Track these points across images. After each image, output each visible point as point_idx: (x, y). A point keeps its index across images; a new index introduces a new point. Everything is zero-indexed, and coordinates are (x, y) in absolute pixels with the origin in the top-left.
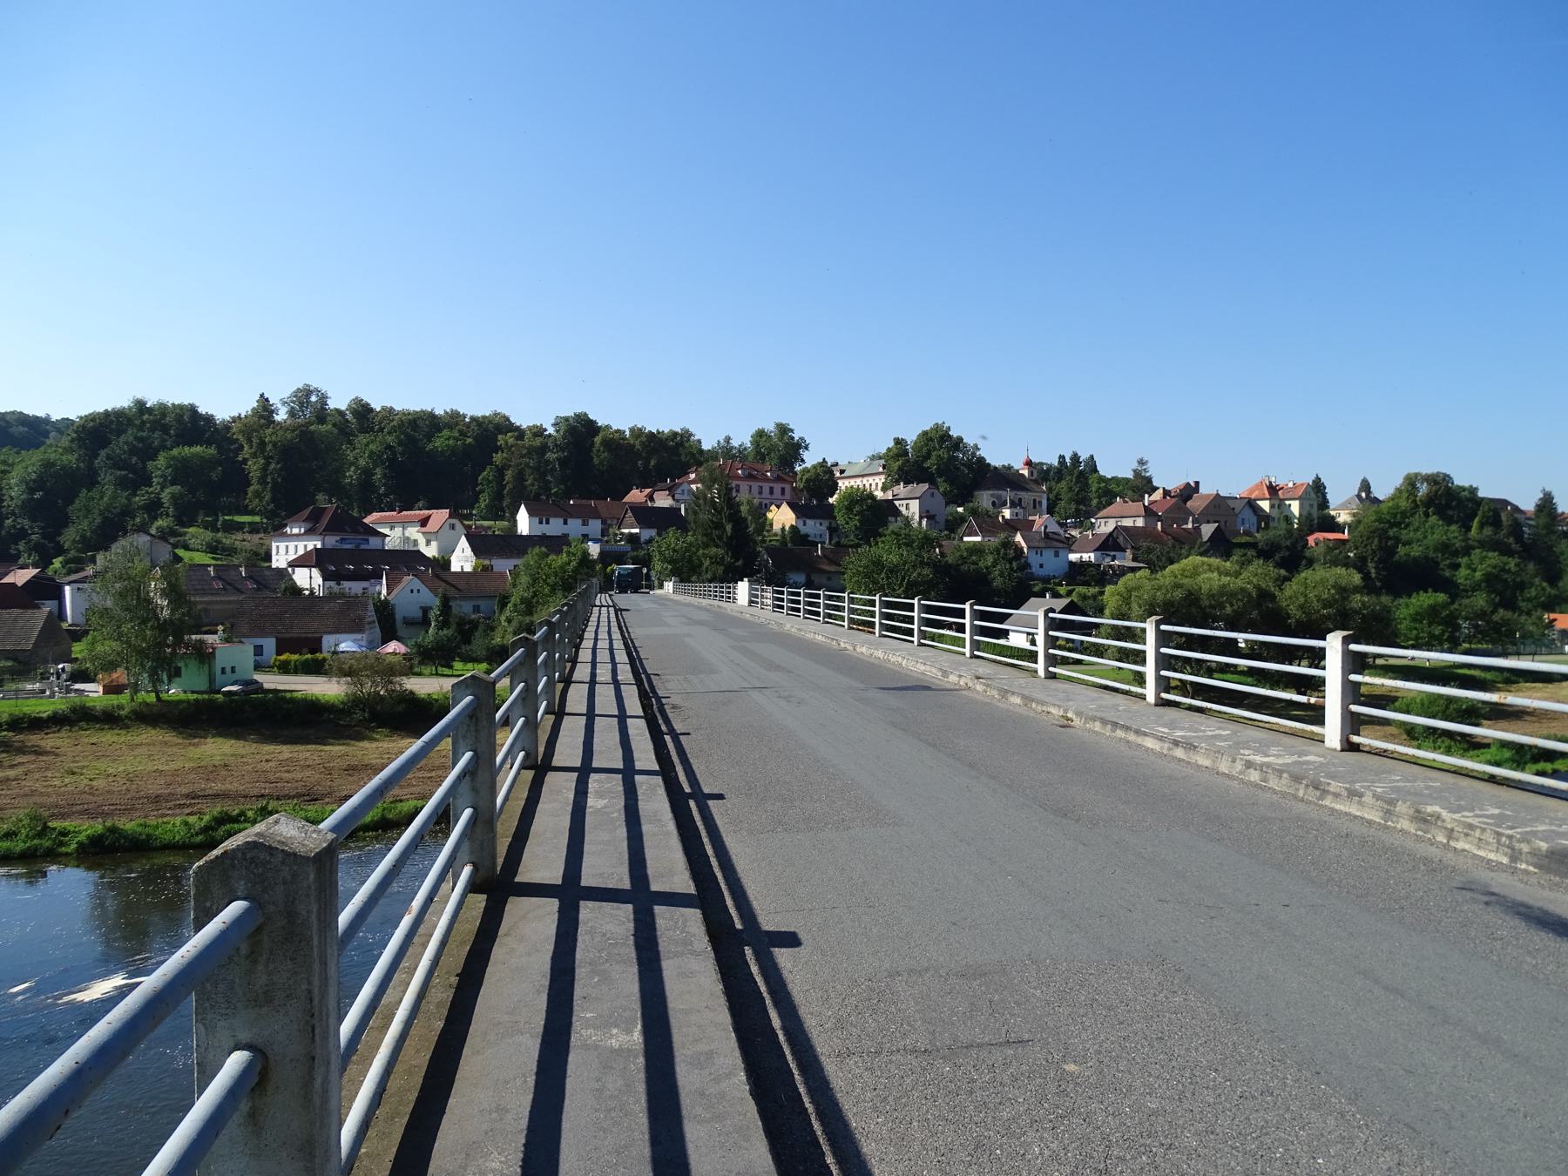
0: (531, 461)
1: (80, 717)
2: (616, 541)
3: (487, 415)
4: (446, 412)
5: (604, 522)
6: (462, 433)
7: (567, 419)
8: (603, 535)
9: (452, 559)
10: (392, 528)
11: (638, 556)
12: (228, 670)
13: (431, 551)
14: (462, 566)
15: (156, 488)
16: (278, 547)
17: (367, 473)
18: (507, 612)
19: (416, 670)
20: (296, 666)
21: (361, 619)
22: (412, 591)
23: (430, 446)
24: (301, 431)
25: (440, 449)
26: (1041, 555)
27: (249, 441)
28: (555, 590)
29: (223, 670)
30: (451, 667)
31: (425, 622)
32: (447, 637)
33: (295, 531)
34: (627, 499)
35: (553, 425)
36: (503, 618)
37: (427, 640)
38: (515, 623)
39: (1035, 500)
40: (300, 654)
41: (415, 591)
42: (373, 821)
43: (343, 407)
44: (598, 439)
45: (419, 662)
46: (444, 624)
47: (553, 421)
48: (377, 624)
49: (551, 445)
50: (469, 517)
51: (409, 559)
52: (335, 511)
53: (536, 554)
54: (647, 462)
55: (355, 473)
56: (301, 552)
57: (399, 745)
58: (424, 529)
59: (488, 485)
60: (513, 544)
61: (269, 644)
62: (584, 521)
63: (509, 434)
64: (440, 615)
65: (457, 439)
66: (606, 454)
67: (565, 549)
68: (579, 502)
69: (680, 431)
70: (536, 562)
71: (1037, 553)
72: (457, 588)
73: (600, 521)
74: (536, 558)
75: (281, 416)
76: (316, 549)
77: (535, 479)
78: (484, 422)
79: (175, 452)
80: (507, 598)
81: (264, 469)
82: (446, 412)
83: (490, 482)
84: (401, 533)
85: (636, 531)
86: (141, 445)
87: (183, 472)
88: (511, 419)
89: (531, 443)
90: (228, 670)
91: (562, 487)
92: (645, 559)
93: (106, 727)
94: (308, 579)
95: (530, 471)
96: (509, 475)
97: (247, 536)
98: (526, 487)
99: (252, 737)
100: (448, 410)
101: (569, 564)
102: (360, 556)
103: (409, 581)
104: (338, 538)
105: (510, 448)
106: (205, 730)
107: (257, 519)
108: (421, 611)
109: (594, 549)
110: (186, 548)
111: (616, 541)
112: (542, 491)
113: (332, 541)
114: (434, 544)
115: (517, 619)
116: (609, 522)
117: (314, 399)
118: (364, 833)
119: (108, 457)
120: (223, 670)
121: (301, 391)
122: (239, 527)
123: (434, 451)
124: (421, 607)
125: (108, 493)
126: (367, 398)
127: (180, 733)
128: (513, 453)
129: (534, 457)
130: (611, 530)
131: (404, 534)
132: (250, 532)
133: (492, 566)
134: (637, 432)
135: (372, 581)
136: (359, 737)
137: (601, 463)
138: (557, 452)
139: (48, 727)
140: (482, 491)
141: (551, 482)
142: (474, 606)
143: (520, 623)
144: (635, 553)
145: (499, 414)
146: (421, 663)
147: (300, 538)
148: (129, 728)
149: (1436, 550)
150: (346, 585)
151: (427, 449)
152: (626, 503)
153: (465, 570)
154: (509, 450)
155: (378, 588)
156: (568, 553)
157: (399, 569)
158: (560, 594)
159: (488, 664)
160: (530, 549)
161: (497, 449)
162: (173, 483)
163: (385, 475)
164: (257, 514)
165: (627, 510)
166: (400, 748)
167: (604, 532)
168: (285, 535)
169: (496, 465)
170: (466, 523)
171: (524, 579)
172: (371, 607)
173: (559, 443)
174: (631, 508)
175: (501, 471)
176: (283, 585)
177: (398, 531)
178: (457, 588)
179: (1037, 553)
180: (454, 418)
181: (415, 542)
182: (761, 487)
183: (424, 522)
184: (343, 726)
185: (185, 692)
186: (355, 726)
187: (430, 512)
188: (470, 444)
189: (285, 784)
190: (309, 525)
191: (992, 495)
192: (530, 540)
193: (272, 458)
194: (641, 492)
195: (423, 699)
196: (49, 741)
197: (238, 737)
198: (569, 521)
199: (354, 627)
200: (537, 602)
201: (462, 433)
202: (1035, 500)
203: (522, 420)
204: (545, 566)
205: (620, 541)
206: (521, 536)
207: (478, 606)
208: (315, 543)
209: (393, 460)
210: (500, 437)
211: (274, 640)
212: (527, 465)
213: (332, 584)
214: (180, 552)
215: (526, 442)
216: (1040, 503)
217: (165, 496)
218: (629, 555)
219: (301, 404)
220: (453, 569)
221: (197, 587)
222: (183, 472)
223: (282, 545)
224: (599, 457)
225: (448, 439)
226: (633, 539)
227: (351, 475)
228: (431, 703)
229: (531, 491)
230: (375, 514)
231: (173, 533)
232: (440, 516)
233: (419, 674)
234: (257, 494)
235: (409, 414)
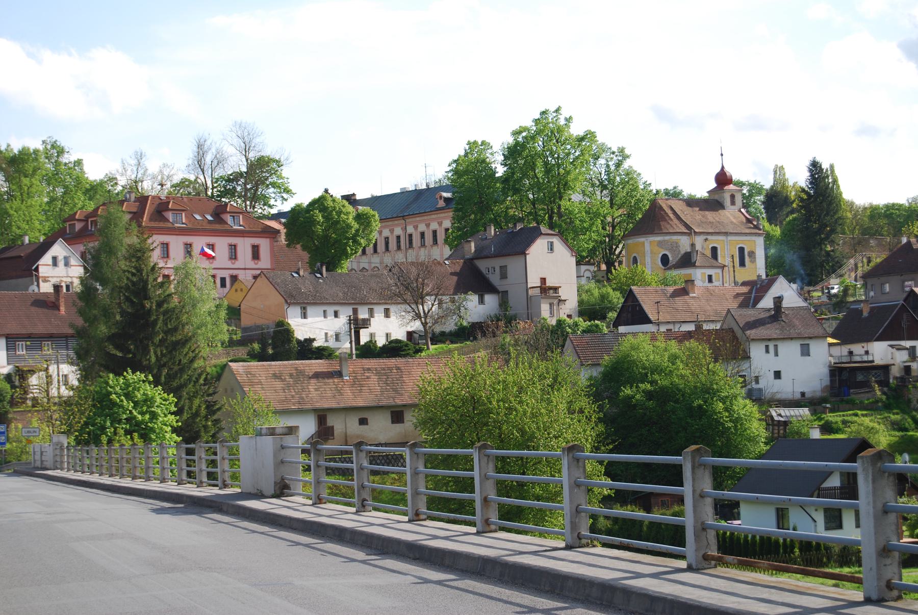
26: (776, 354)
39: (741, 250)
69: (41, 147)
71: (767, 351)
126: (597, 134)
149: (831, 390)
179: (767, 351)
182: (552, 244)
191: (660, 244)
202: (741, 250)
216: (752, 254)
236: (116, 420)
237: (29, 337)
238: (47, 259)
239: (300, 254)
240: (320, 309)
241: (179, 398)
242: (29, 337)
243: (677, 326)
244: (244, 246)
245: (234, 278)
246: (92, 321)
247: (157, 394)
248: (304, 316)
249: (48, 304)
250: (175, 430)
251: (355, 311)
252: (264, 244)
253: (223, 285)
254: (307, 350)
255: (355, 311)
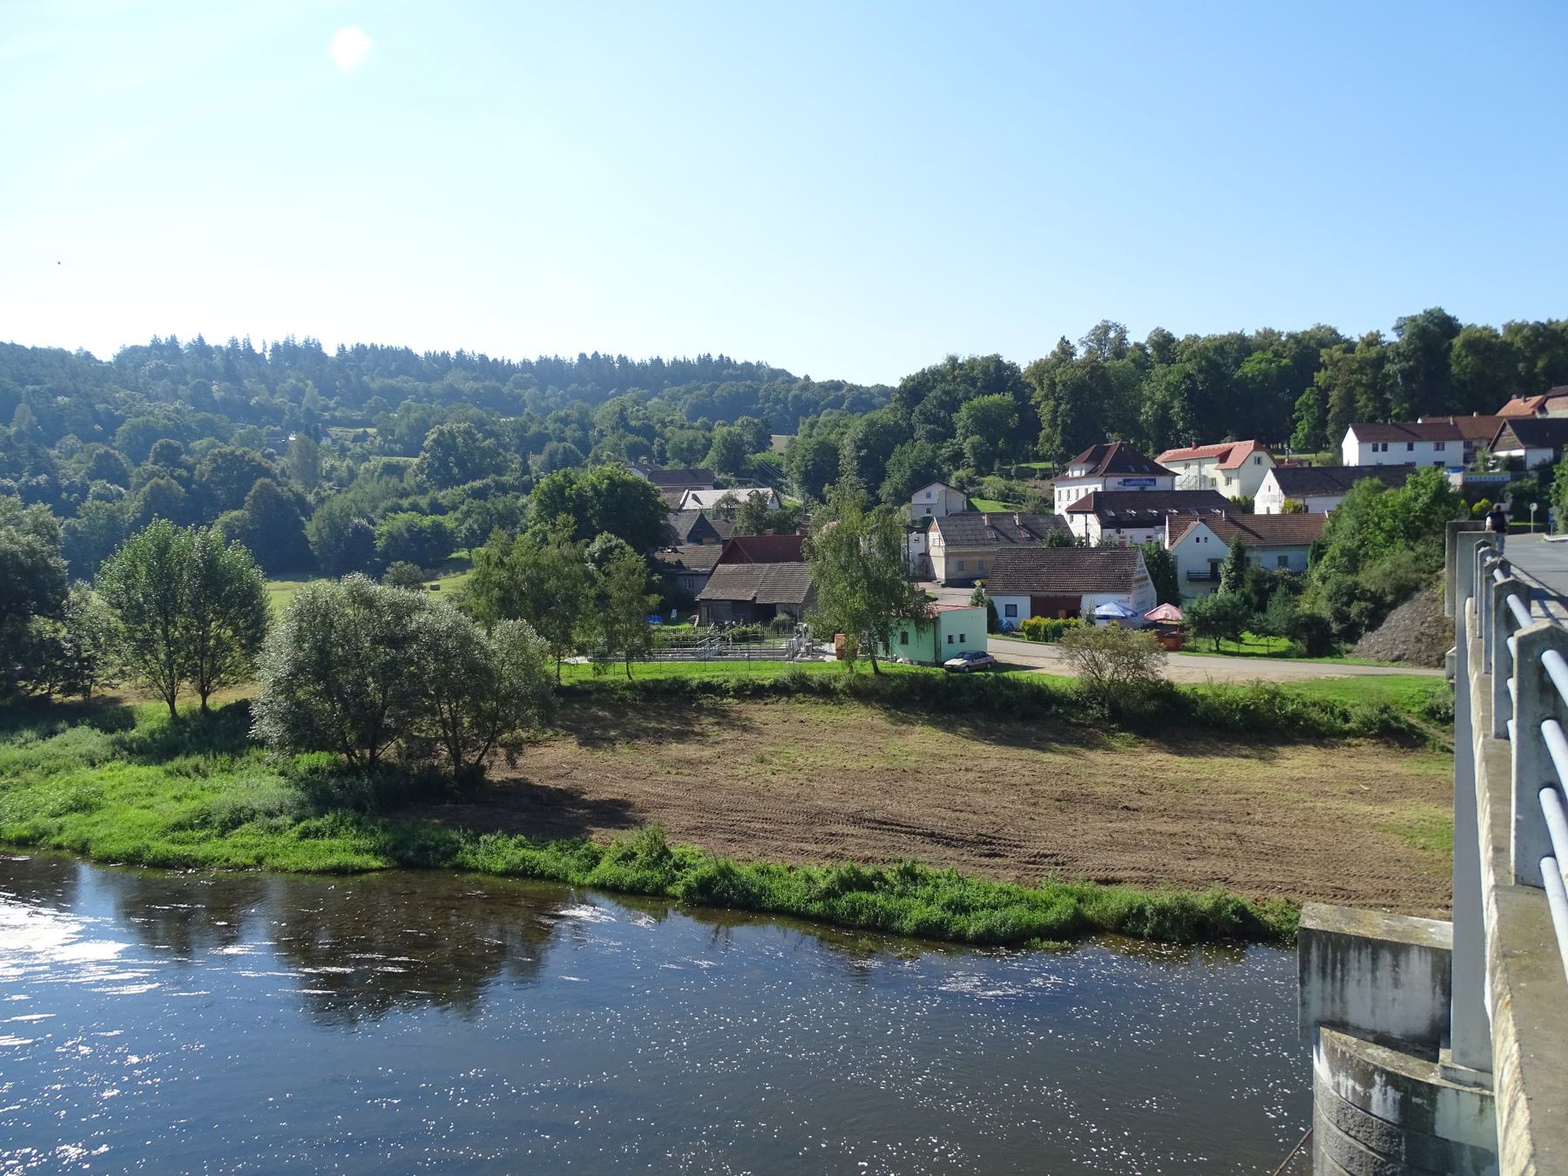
0: (1364, 377)
1: (798, 688)
2: (1487, 469)
3: (1308, 329)
4: (1258, 332)
5: (1468, 445)
6: (1277, 354)
7: (1413, 319)
8: (1466, 460)
9: (1255, 499)
10: (1187, 466)
11: (1521, 488)
12: (956, 639)
13: (1230, 491)
14: (1268, 508)
15: (959, 439)
16: (1060, 492)
17: (1165, 407)
18: (1322, 568)
19: (1191, 644)
20: (1046, 632)
21: (1127, 575)
22: (1198, 540)
23: (1239, 373)
24: (1092, 367)
25: (1250, 375)
27: (1041, 383)
28: (1393, 537)
29: (950, 639)
30: (1239, 641)
31: (1214, 577)
32: (1232, 602)
33: (1077, 473)
34: (1504, 412)
35: (1396, 329)
36: (1315, 575)
37: (1204, 607)
38: (1330, 585)
40: (1052, 618)
41: (1202, 539)
42: (1057, 920)
43: (1143, 341)
44: (1457, 342)
45: (1194, 633)
46: (1235, 585)
47: (1394, 324)
48: (1150, 581)
49: (1391, 354)
50: (1282, 452)
51: (1203, 501)
52: (1119, 448)
53: (1365, 488)
54: (1532, 362)
55: (1151, 408)
56: (1082, 495)
57: (1144, 764)
58: (1224, 466)
59: (1307, 410)
60: (1337, 478)
61: (1024, 603)
62: (1438, 445)
63: (1335, 347)
64: (1232, 570)
65: (1270, 361)
66: (1469, 358)
67: (1410, 477)
68: (1430, 420)
70: (1364, 499)
72: (1257, 535)
73: (1461, 443)
74: (1365, 493)
75: (1081, 353)
76: (1096, 493)
77: (1369, 399)
78: (1304, 339)
79: (975, 402)
80: (1321, 547)
81: (1055, 411)
82: (1258, 332)
83: (1310, 407)
84: (1197, 471)
85: (1520, 452)
86: (948, 399)
87: (986, 423)
88: (1339, 332)
89: (1363, 355)
90: (956, 639)
91: (1406, 405)
92: (1533, 491)
93: (821, 700)
94: (1086, 528)
95: (1362, 390)
96: (1334, 396)
97: (1039, 483)
98: (1357, 409)
99: (964, 729)
100: (1261, 330)
101: (1416, 499)
102: (1144, 499)
103: (1196, 527)
104: (1121, 479)
105: (1335, 364)
106: (916, 714)
107: (1049, 465)
108: (1209, 564)
109: (1456, 480)
110: (982, 497)
111: (1487, 469)
112: (1378, 413)
113: (1114, 483)
114: (1235, 482)
115: (1337, 578)
116: (1475, 444)
117: (1112, 335)
118: (1042, 941)
119: (921, 413)
120: (950, 639)
121: (1100, 328)
122: (1031, 474)
123: (1244, 378)
124: (1209, 560)
125: (917, 450)
126: (1168, 329)
127: (890, 716)
128: (1339, 370)
129: (1368, 371)
130: (1479, 455)
131: (1200, 472)
132: (1043, 478)
133: (1307, 507)
134: (1514, 329)
135: (1157, 527)
136: (1091, 744)
137: (1463, 370)
138: (1400, 362)
139: (769, 697)
140: (1300, 419)
141: (1389, 400)
142: (1280, 557)
143: (1339, 585)
144: (1518, 483)
145: (1323, 327)
146: (1196, 635)
147: (1081, 481)
148: (842, 704)
150: (1127, 532)
151: (1235, 377)
152: (1502, 418)
153: (1271, 513)
154: (1336, 366)
155: (1160, 536)
156: (1415, 484)
157: (1189, 513)
158: (1400, 543)
159: (1290, 640)
160: (1356, 482)
161: (1320, 367)
162: (973, 433)
163: (1183, 408)
164: (1049, 460)
165: (1505, 425)
166: (1141, 768)
167: (1467, 459)
168: (1067, 479)
169: (1317, 386)
170: (1276, 457)
171: (1348, 523)
172: (1141, 560)
173: (1402, 350)
174: (1509, 421)
175: (1324, 394)
176: (1049, 535)
177: (1194, 469)
178: (1257, 535)
180: (1268, 339)
181: (1214, 480)
183: (1223, 457)
184: (1075, 725)
185: (912, 663)
186: (1090, 726)
187: (1231, 445)
188: (1286, 366)
189: (971, 816)
190: (1091, 467)
192: (1359, 472)
193: (1062, 398)
194: (1525, 401)
195: (1185, 694)
196: (759, 713)
197: (949, 727)
198: (1416, 445)
199: (1119, 585)
200: (1366, 555)
201: (1277, 354)
203: (1353, 331)
204: (1377, 504)
205: (1493, 468)
206: (1348, 468)
207: (1286, 557)
208: (1096, 486)
209: (1192, 391)
210: (1323, 351)
211: (1028, 599)
212: (1359, 383)
213: (1112, 531)
214: (976, 502)
215: (1358, 355)
217: (966, 447)
218: (1508, 487)
219: (1099, 341)
220: (1257, 512)
221: (969, 538)
222: (986, 423)
223: (1064, 490)
224: (1460, 363)
225: (1260, 362)
226: (1514, 465)
227: (1147, 412)
228: (1194, 702)
229: (1363, 414)
230: (1168, 452)
231: (972, 482)
232: (1242, 449)
233: (1194, 650)
234: (1049, 439)
235: (1215, 339)
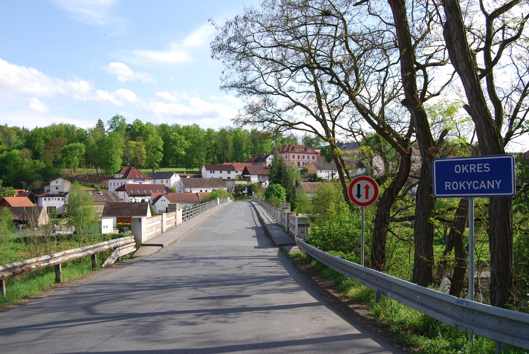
236: (274, 193)
237: (262, 175)
238: (268, 158)
239: (323, 158)
240: (324, 171)
241: (287, 189)
242: (262, 175)
243: (77, 251)
244: (311, 156)
245: (308, 163)
246: (271, 173)
247: (282, 188)
248: (321, 172)
249: (266, 168)
250: (286, 195)
251: (332, 171)
252: (315, 156)
253: (306, 164)
254: (320, 179)
255: (332, 171)
